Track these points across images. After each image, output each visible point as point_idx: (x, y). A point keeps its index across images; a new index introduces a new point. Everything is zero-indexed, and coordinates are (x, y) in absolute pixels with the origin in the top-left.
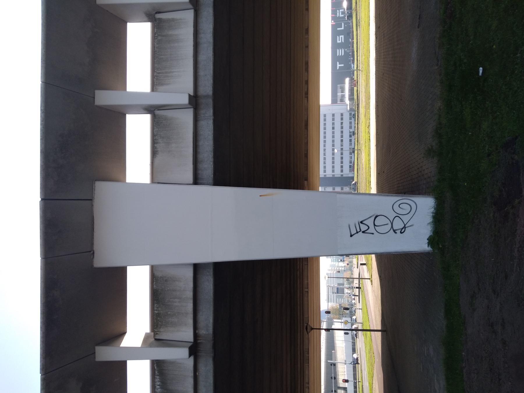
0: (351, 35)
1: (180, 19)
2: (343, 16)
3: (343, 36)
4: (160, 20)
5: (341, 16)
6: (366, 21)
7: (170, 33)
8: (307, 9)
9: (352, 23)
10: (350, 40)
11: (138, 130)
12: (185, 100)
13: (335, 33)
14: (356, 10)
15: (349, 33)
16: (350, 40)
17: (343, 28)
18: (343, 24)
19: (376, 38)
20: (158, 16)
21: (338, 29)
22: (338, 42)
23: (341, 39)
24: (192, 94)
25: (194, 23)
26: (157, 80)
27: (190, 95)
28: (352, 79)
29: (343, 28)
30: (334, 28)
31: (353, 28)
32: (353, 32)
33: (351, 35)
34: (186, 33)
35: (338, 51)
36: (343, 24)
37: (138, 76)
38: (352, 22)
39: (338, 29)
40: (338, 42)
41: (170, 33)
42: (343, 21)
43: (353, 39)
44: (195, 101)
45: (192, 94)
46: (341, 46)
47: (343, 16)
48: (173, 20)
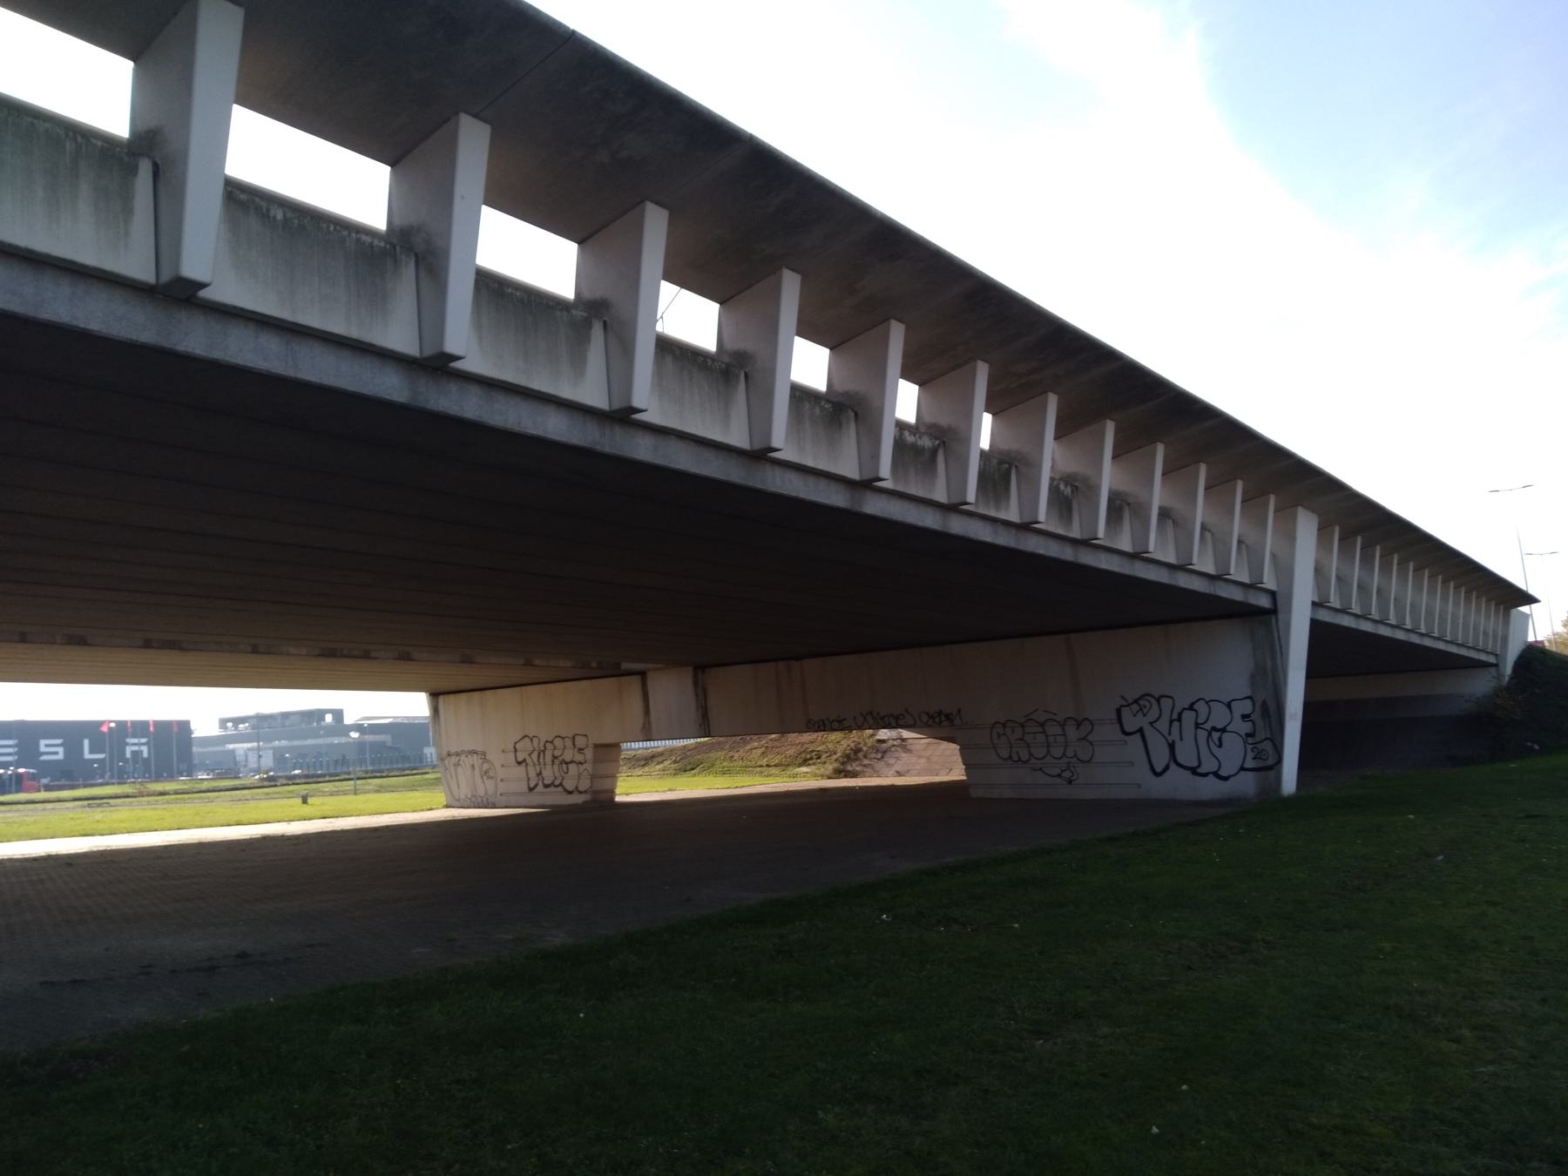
0: (63, 782)
1: (127, 234)
2: (128, 755)
3: (60, 756)
4: (133, 170)
5: (129, 750)
6: (101, 826)
7: (85, 188)
8: (147, 644)
9: (101, 785)
10: (45, 781)
11: (349, 185)
12: (193, 268)
13: (72, 733)
14: (141, 795)
15: (69, 774)
16: (45, 781)
17: (87, 756)
18: (101, 756)
19: (35, 859)
20: (145, 168)
21: (86, 742)
22: (43, 743)
23: (51, 750)
24: (203, 293)
25: (111, 273)
26: (246, 202)
27: (203, 286)
28: (34, 777)
29: (87, 756)
30: (90, 729)
31: (85, 786)
32: (73, 787)
33: (63, 782)
34: (76, 236)
35: (11, 742)
36: (101, 756)
37: (272, 153)
38: (107, 784)
39: (86, 742)
40: (43, 743)
41: (85, 188)
42: (111, 757)
43: (48, 788)
44: (181, 294)
45: (203, 293)
46: (72, 747)
47: (128, 755)
48: (128, 210)
